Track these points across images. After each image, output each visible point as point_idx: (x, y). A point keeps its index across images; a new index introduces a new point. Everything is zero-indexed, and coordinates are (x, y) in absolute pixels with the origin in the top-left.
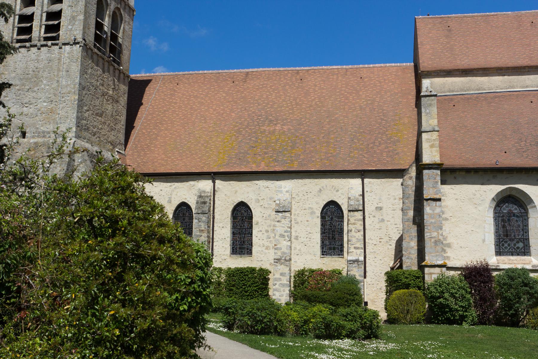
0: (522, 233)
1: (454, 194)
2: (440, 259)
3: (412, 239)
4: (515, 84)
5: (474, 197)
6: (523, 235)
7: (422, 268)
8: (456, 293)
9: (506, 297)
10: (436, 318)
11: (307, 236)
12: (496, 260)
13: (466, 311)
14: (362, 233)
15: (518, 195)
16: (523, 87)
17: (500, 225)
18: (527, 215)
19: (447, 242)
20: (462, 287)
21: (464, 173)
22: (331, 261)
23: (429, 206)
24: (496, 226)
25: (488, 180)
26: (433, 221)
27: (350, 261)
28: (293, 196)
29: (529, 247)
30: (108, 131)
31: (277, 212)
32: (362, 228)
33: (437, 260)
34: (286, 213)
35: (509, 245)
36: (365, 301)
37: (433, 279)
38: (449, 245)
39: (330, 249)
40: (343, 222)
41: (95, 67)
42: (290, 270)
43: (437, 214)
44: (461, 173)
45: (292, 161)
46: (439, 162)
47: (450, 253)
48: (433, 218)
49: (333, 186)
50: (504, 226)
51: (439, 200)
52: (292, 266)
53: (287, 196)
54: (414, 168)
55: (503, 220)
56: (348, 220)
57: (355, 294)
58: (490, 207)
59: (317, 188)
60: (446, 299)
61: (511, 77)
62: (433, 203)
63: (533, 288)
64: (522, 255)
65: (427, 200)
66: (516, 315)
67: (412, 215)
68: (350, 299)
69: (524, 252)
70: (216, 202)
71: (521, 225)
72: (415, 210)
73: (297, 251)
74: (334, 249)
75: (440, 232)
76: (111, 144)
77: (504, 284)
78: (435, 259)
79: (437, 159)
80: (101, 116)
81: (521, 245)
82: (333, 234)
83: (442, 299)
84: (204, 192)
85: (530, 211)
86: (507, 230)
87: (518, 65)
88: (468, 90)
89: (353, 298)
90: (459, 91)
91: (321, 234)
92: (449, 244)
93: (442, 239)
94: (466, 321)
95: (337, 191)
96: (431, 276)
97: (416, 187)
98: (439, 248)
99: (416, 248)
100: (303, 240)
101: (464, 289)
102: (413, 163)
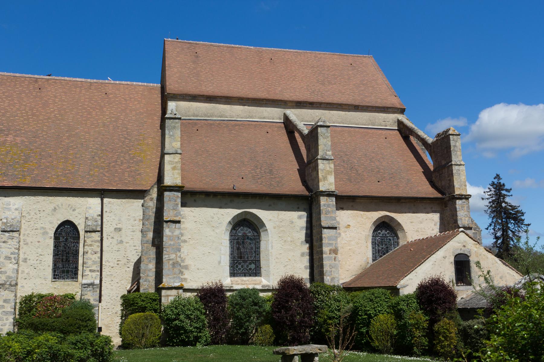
0: (254, 255)
1: (194, 217)
2: (177, 281)
3: (150, 261)
4: (254, 114)
6: (255, 257)
7: (159, 290)
8: (191, 315)
9: (238, 316)
10: (171, 340)
11: (37, 258)
13: (200, 332)
14: (99, 255)
15: (255, 222)
16: (261, 118)
18: (259, 238)
19: (185, 264)
20: (197, 308)
21: (203, 196)
22: (64, 285)
23: (169, 227)
25: (226, 204)
26: (172, 243)
27: (85, 284)
28: (23, 215)
29: (260, 268)
32: (99, 250)
33: (174, 282)
34: (14, 233)
35: (242, 266)
36: (99, 326)
37: (169, 301)
38: (186, 267)
39: (63, 272)
40: (79, 243)
42: (16, 296)
45: (24, 176)
48: (171, 240)
49: (69, 205)
50: (238, 249)
51: (179, 222)
52: (18, 291)
53: (16, 214)
54: (155, 190)
56: (85, 241)
57: (88, 320)
58: (227, 230)
59: (52, 207)
60: (181, 321)
61: (250, 108)
62: (173, 225)
64: (253, 276)
66: (246, 333)
68: (82, 326)
69: (256, 273)
71: (254, 247)
72: (154, 232)
73: (25, 274)
74: (68, 272)
75: (179, 254)
77: (236, 304)
78: (172, 281)
79: (178, 181)
81: (253, 266)
82: (67, 256)
83: (177, 321)
85: (262, 234)
86: (241, 252)
87: (257, 97)
88: (211, 117)
89: (86, 324)
90: (202, 117)
91: (54, 256)
92: (187, 266)
93: (180, 262)
94: (199, 342)
95: (74, 210)
96: (168, 298)
97: (156, 208)
98: (176, 270)
99: (154, 270)
100: (32, 262)
101: (199, 310)
102: (155, 184)
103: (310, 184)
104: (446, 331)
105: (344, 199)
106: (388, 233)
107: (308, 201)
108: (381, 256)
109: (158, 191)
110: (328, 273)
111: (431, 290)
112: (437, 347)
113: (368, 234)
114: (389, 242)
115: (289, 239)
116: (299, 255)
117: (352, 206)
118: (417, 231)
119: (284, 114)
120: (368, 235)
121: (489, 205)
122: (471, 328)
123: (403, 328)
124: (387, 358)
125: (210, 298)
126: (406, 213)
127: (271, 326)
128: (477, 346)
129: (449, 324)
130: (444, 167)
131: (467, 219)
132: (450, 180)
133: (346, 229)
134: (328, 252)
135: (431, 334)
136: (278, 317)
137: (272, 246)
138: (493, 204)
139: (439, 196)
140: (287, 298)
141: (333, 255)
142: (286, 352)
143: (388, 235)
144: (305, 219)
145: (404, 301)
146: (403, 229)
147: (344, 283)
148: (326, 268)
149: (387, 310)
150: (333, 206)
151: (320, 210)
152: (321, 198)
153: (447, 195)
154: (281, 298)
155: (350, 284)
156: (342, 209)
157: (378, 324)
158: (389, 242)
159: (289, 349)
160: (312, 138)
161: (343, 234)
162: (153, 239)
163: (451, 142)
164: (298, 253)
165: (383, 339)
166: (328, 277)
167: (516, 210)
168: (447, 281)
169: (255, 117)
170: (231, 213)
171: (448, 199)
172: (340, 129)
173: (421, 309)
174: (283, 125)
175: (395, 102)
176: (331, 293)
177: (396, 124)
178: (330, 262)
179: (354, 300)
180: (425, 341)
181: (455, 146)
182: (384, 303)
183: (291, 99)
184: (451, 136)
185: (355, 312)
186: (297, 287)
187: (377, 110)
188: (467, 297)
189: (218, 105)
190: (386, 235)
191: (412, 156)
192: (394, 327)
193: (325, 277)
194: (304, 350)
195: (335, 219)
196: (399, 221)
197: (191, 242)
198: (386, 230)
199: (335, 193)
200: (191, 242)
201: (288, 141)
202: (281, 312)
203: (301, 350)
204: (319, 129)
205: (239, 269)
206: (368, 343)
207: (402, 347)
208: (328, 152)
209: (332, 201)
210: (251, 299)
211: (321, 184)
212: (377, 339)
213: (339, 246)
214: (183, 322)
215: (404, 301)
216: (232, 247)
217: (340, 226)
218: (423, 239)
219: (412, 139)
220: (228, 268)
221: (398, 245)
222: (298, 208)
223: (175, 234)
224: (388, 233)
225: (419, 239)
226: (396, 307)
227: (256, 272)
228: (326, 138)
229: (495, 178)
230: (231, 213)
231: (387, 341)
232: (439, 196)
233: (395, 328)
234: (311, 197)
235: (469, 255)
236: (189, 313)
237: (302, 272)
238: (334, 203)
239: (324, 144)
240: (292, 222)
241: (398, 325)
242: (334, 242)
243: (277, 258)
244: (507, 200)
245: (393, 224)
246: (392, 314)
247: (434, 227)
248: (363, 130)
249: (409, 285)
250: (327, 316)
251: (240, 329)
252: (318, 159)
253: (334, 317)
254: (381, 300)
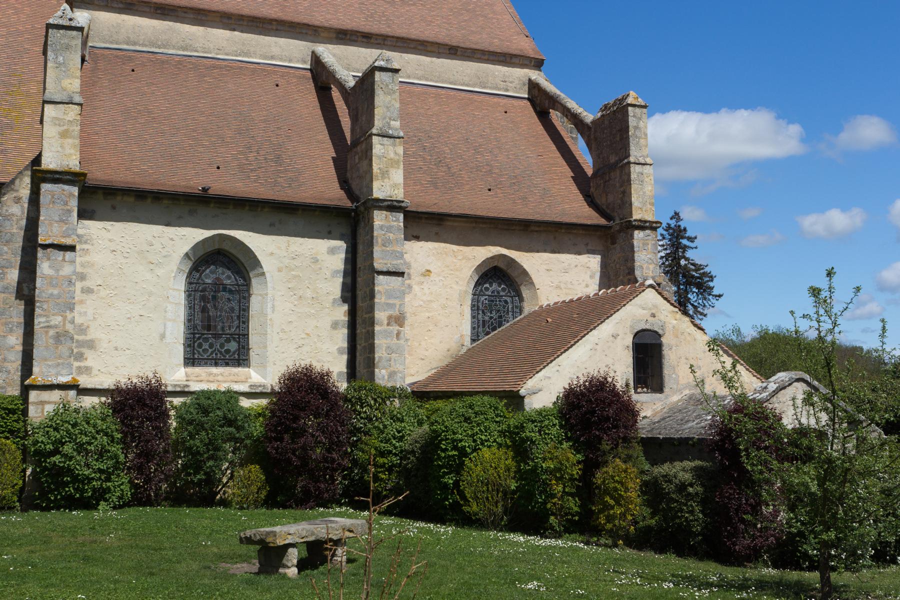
0: (236, 322)
1: (110, 240)
2: (64, 372)
3: (11, 330)
4: (252, 49)
5: (148, 248)
6: (238, 327)
7: (26, 390)
8: (90, 444)
9: (190, 448)
10: (44, 495)
12: (184, 374)
13: (108, 479)
15: (233, 251)
16: (265, 58)
17: (197, 307)
18: (248, 291)
19: (88, 338)
20: (102, 430)
21: (132, 199)
23: (49, 259)
24: (190, 308)
25: (180, 217)
26: (56, 292)
29: (249, 349)
33: (58, 374)
35: (211, 346)
37: (46, 414)
38: (91, 345)
44: (126, 198)
46: (77, 169)
47: (91, 360)
48: (54, 286)
50: (204, 310)
51: (72, 248)
54: (27, 180)
55: (203, 298)
58: (180, 270)
60: (65, 456)
61: (245, 35)
62: (59, 255)
63: (243, 428)
64: (234, 366)
65: (45, 247)
66: (211, 481)
67: (16, 280)
69: (238, 360)
71: (237, 308)
72: (22, 268)
75: (69, 316)
77: (190, 423)
78: (53, 371)
79: (73, 163)
81: (233, 346)
83: (58, 456)
85: (254, 282)
86: (209, 316)
87: (260, 15)
88: (165, 47)
90: (146, 46)
92: (92, 341)
93: (71, 331)
94: (106, 500)
96: (42, 408)
97: (28, 219)
98: (63, 349)
99: (20, 348)
101: (106, 434)
102: (26, 168)
103: (354, 185)
104: (619, 486)
105: (421, 218)
106: (503, 290)
107: (348, 218)
108: (488, 333)
109: (32, 182)
110: (383, 363)
111: (591, 401)
112: (598, 518)
113: (464, 289)
114: (504, 307)
115: (309, 293)
116: (328, 325)
117: (437, 234)
118: (558, 287)
119: (313, 52)
120: (466, 292)
121: (661, 262)
122: (670, 481)
123: (530, 478)
124: (496, 539)
125: (133, 409)
126: (538, 252)
127: (261, 468)
128: (679, 517)
129: (625, 471)
130: (613, 167)
131: (651, 267)
132: (624, 192)
133: (422, 279)
134: (386, 322)
135: (586, 489)
136: (277, 449)
137: (273, 306)
138: (667, 260)
139: (603, 221)
140: (296, 412)
141: (395, 328)
142: (269, 540)
143: (502, 293)
144: (343, 256)
145: (533, 422)
146: (532, 283)
147: (413, 384)
148: (380, 353)
149: (499, 440)
150: (399, 230)
151: (372, 237)
152: (376, 213)
153: (618, 222)
154: (284, 412)
155: (427, 385)
156: (417, 238)
157: (479, 468)
158: (504, 307)
159: (274, 534)
160: (363, 91)
161: (416, 288)
162: (19, 283)
163: (631, 119)
164: (327, 322)
165: (487, 498)
166: (383, 371)
167: (702, 271)
168: (620, 385)
169: (255, 54)
170: (190, 237)
171: (618, 228)
172: (420, 89)
173: (568, 439)
174: (309, 74)
175: (524, 45)
176: (388, 402)
177: (526, 88)
178: (388, 341)
179: (433, 418)
180: (573, 505)
181: (636, 128)
182: (493, 426)
183: (326, 25)
184: (630, 109)
185: (432, 444)
186: (318, 389)
187: (491, 58)
188: (654, 415)
189: (178, 25)
190: (498, 292)
191: (554, 147)
192: (512, 474)
193: (376, 370)
194: (313, 534)
195: (402, 257)
196: (525, 267)
197: (103, 293)
198: (499, 283)
199: (403, 205)
200: (103, 293)
201: (317, 104)
202: (281, 440)
203: (304, 533)
204: (378, 76)
205: (205, 351)
206: (456, 506)
207: (526, 516)
208: (392, 123)
209: (397, 220)
210: (219, 413)
211: (376, 185)
212: (476, 498)
213: (408, 310)
214: (71, 459)
215: (533, 422)
216: (191, 307)
217: (412, 271)
218: (571, 301)
219: (555, 116)
220: (181, 348)
221: (521, 312)
222: (330, 233)
223: (61, 273)
224: (503, 290)
225: (564, 302)
226: (518, 433)
227: (240, 357)
228: (389, 94)
229: (671, 219)
230: (190, 237)
231: (497, 503)
232: (603, 221)
233: (514, 478)
234: (356, 210)
235: (661, 332)
236: (85, 439)
237: (331, 361)
238: (402, 224)
239: (386, 106)
240: (316, 261)
241: (519, 471)
242: (397, 302)
243: (283, 331)
244: (689, 254)
245: (513, 274)
246: (508, 447)
247: (590, 281)
248: (463, 94)
249: (545, 389)
250: (376, 449)
251: (196, 473)
252: (372, 135)
253: (390, 452)
254: (486, 419)
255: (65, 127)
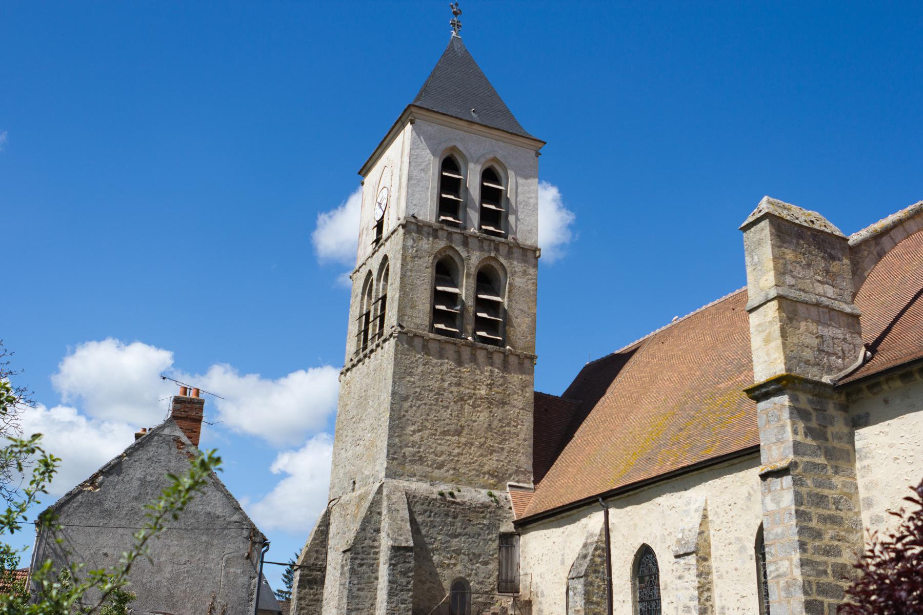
11: (738, 604)
30: (481, 455)
31: (677, 556)
41: (435, 361)
43: (784, 509)
70: (612, 553)
76: (492, 475)
80: (458, 433)
84: (592, 535)
255: (767, 331)
